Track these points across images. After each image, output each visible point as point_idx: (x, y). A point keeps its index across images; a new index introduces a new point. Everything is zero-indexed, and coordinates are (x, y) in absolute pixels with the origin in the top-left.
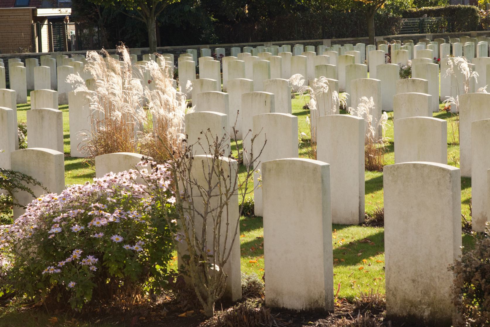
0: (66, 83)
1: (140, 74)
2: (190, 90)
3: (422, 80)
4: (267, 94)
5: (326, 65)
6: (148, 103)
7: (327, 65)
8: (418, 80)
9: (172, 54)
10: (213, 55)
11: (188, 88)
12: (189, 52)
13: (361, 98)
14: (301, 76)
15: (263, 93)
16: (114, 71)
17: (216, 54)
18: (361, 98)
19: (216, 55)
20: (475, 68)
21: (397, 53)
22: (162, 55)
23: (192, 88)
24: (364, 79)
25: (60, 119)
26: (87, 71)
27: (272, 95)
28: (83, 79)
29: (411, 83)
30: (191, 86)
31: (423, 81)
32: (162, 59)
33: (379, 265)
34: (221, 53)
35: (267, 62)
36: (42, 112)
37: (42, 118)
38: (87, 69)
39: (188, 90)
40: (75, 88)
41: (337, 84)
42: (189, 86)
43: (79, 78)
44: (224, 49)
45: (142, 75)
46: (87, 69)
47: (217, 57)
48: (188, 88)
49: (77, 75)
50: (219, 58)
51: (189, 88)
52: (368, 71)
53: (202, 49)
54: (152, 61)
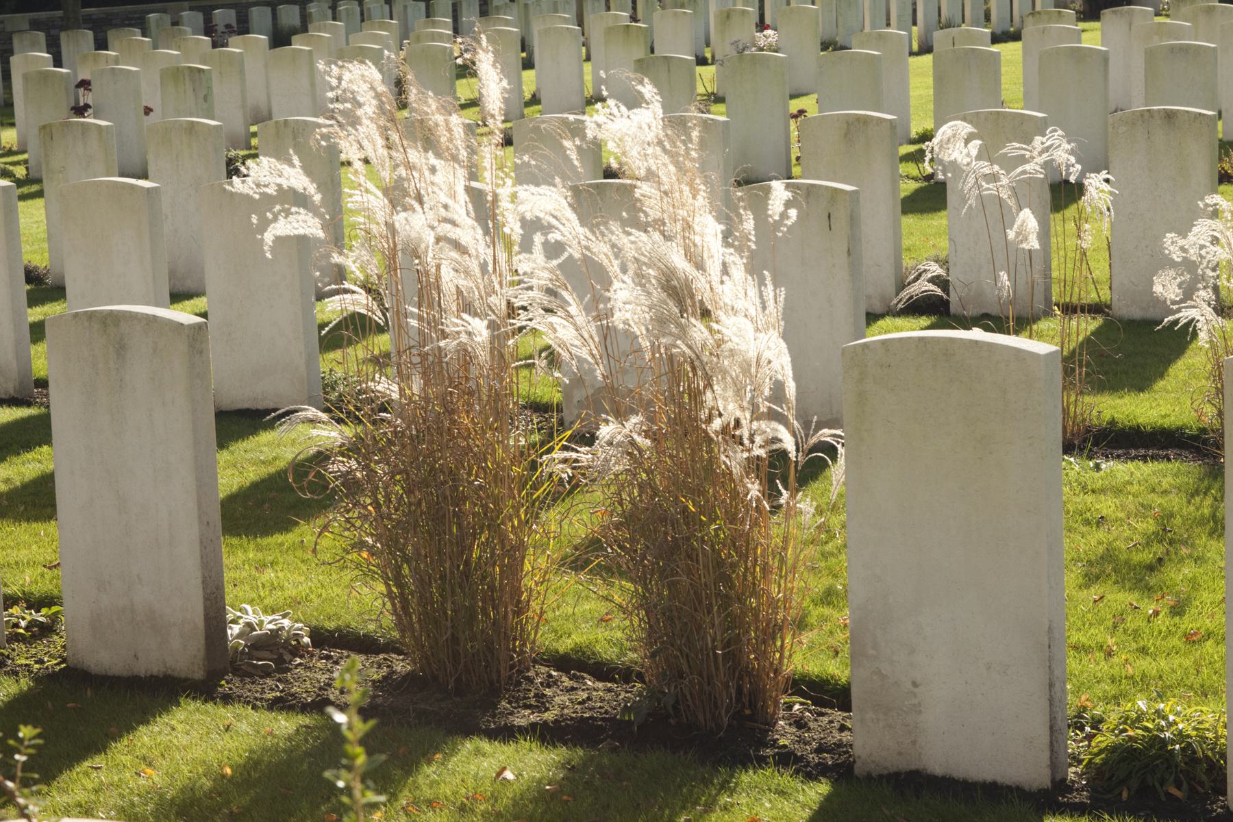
0: (232, 194)
1: (567, 159)
2: (789, 222)
3: (1200, 114)
5: (666, 57)
6: (607, 283)
8: (1187, 112)
10: (209, 30)
11: (777, 218)
13: (1202, 199)
14: (969, 128)
15: (821, 186)
16: (429, 142)
18: (1202, 199)
21: (725, 15)
22: (646, 80)
23: (793, 213)
24: (991, 113)
25: (201, 352)
26: (323, 143)
27: (853, 191)
28: (312, 182)
29: (1159, 122)
30: (788, 204)
31: (1204, 115)
32: (648, 96)
33: (589, 526)
35: (445, 47)
37: (121, 349)
41: (895, 127)
42: (782, 208)
43: (296, 178)
45: (576, 163)
46: (325, 137)
47: (219, 32)
48: (777, 218)
49: (292, 165)
51: (784, 215)
52: (588, 59)
54: (611, 102)
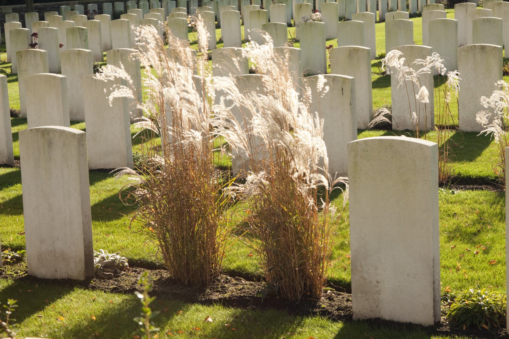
2: (326, 92)
3: (495, 47)
4: (345, 78)
5: (275, 24)
7: (277, 24)
8: (490, 46)
9: (56, 12)
11: (321, 90)
12: (76, 8)
13: (496, 82)
15: (339, 77)
17: (89, 10)
18: (496, 82)
19: (89, 11)
20: (457, 24)
23: (327, 88)
26: (133, 59)
27: (352, 79)
28: (129, 75)
29: (478, 50)
30: (325, 84)
31: (497, 47)
32: (267, 40)
34: (94, 9)
36: (48, 134)
37: (50, 144)
38: (134, 56)
39: (321, 93)
40: (109, 93)
42: (323, 86)
43: (122, 73)
44: (96, 5)
45: (238, 67)
48: (321, 90)
49: (120, 68)
50: (92, 13)
51: (324, 89)
52: (243, 24)
53: (76, 5)
